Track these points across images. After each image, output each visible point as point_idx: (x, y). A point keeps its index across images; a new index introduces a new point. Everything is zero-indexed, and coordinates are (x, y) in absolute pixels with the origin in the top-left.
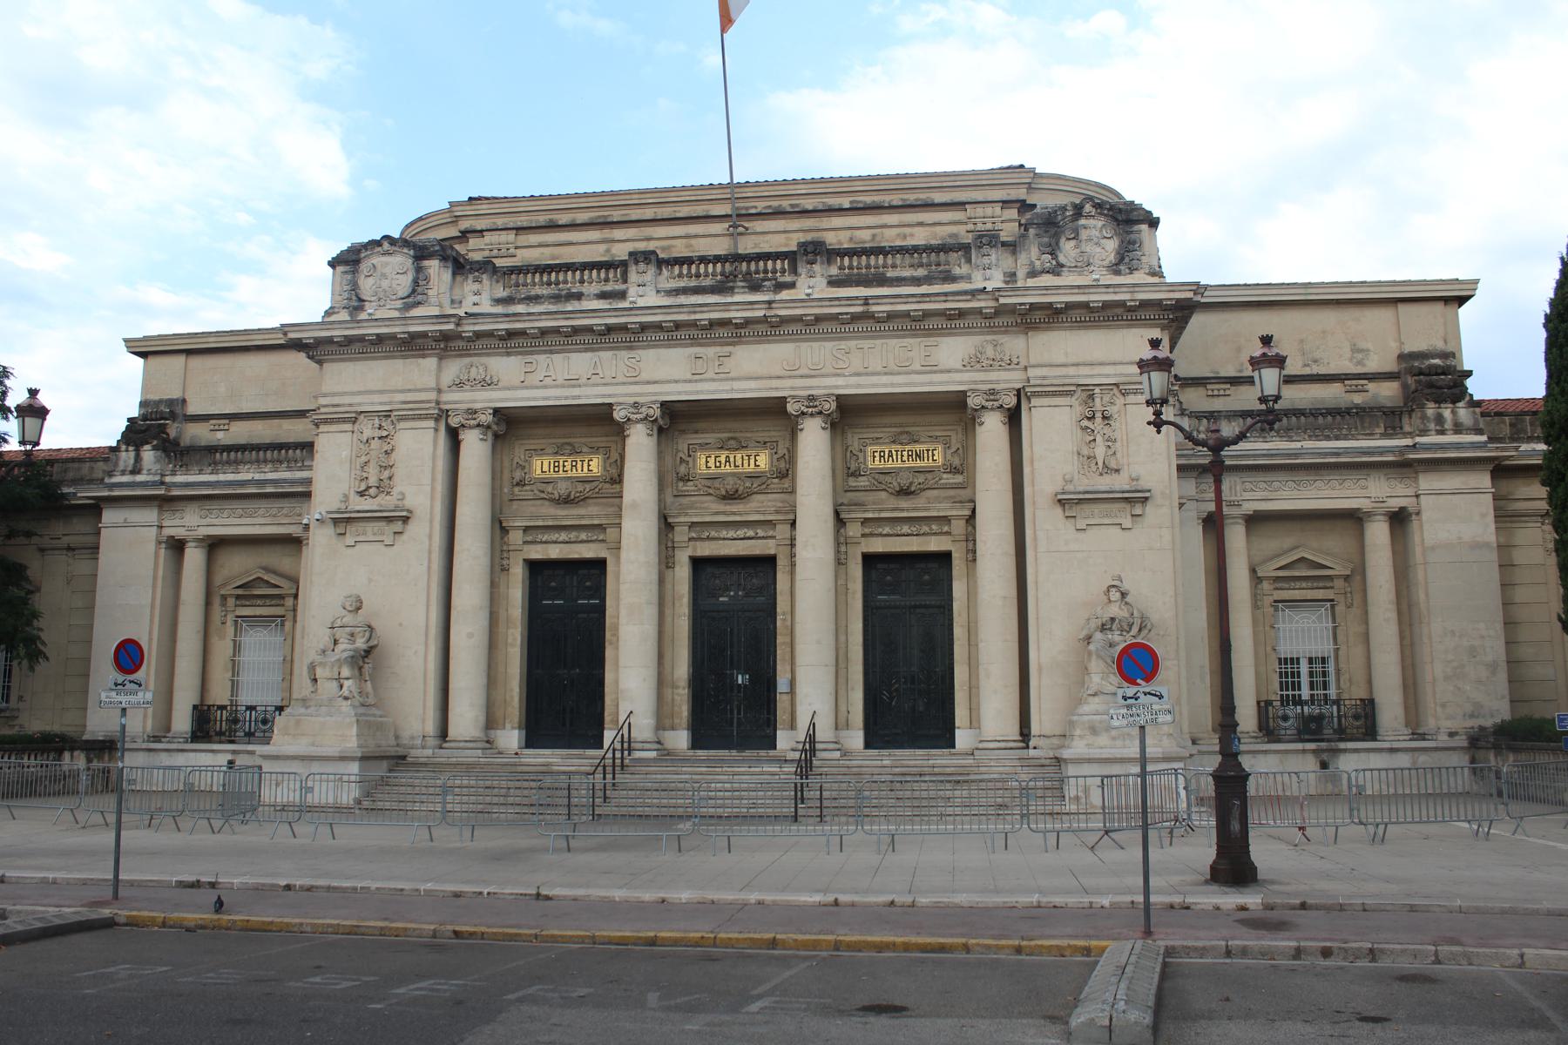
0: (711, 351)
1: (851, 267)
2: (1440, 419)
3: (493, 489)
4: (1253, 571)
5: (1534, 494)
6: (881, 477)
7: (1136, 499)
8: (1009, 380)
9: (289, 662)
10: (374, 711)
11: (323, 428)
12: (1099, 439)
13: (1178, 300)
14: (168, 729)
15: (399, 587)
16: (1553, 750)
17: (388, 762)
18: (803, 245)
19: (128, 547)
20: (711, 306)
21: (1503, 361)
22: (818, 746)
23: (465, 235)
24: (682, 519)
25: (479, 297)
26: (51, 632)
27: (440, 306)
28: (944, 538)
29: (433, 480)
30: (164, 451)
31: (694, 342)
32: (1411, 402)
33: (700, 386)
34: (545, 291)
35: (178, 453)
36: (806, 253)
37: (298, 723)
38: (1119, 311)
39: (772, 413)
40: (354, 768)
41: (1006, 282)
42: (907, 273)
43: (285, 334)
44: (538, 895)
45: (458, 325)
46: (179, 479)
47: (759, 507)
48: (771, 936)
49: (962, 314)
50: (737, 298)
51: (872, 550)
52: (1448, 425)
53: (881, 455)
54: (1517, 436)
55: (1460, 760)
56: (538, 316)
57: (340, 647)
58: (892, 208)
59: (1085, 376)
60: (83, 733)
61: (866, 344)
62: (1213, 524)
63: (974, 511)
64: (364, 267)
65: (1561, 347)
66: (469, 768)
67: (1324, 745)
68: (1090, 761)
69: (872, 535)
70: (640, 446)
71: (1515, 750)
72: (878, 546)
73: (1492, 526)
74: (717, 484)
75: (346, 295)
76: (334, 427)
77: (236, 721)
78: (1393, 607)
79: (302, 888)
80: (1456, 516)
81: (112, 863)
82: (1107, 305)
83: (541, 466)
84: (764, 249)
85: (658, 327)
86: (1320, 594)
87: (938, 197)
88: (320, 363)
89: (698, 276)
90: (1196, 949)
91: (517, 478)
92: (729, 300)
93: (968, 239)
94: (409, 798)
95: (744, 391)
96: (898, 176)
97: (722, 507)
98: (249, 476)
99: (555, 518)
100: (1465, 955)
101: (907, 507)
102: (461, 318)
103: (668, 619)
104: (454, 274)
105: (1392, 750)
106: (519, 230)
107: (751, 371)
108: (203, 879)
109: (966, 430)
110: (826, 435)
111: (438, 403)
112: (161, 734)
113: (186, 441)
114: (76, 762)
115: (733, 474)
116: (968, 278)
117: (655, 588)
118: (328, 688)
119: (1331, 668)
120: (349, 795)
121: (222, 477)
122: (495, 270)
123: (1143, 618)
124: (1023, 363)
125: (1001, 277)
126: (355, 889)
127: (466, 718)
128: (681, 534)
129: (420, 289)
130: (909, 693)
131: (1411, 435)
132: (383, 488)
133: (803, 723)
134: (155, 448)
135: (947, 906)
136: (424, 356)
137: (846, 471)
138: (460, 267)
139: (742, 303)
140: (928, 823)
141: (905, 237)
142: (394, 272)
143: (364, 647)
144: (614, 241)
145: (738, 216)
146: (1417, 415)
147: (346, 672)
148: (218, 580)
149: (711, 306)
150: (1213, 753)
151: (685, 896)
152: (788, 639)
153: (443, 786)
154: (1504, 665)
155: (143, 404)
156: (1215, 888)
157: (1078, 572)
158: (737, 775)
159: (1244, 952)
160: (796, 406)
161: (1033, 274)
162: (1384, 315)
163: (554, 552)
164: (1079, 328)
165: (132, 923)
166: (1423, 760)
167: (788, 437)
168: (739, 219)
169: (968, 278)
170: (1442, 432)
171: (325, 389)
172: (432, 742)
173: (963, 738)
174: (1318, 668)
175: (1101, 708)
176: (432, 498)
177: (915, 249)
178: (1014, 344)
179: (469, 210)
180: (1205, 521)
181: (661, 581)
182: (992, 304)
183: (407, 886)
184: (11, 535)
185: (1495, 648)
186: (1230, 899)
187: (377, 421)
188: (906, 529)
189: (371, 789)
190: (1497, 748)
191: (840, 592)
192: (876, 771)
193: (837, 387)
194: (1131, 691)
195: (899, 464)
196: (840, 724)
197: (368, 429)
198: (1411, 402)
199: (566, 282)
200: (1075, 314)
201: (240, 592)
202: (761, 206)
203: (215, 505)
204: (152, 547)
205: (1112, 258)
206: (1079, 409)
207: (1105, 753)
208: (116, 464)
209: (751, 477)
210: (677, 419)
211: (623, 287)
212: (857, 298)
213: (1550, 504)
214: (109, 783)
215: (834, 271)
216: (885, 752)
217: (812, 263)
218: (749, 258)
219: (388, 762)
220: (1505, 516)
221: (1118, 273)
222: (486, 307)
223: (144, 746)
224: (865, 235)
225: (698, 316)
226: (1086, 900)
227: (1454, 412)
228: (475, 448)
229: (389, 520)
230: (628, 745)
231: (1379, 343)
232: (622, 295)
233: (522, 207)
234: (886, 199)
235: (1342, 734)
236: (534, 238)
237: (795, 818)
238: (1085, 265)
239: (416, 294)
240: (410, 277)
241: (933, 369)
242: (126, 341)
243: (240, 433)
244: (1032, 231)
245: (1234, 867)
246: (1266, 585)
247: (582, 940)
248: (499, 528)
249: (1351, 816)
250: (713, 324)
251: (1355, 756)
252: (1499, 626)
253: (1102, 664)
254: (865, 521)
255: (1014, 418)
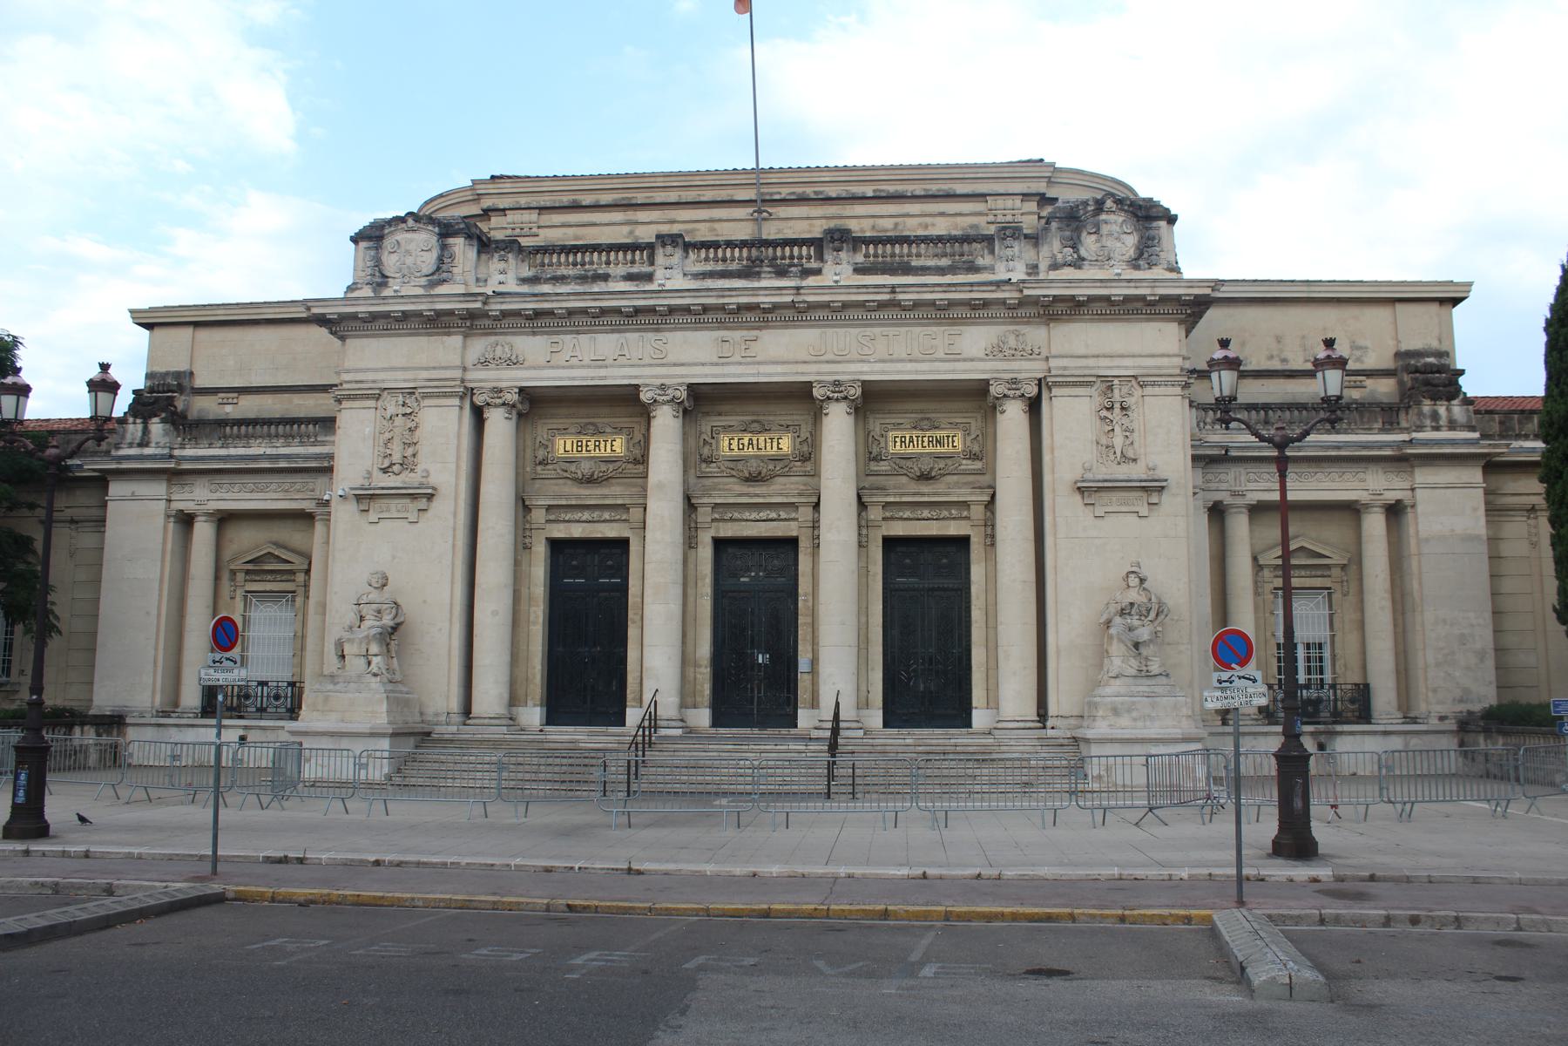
0: (737, 335)
1: (876, 256)
2: (1435, 416)
3: (517, 467)
4: (1255, 559)
5: (1531, 489)
6: (903, 463)
7: (1152, 488)
8: (1030, 369)
9: (300, 640)
10: (401, 687)
11: (345, 404)
12: (1117, 429)
13: (1196, 296)
14: (176, 704)
15: (418, 568)
16: (1544, 734)
17: (415, 738)
18: (830, 232)
19: (136, 521)
20: (739, 291)
21: (1501, 360)
22: (842, 725)
23: (487, 213)
24: (706, 500)
25: (504, 276)
26: (62, 603)
27: (466, 284)
28: (963, 522)
29: (458, 458)
30: (173, 423)
31: (721, 325)
32: (1407, 399)
33: (726, 370)
34: (571, 271)
35: (186, 426)
36: (833, 240)
37: (326, 699)
38: (1139, 305)
39: (799, 398)
40: (385, 744)
41: (1029, 274)
42: (931, 263)
43: (309, 309)
44: (630, 869)
45: (485, 303)
46: (189, 452)
47: (782, 489)
48: (882, 907)
49: (986, 304)
50: (764, 283)
51: (722, 534)
52: (1443, 422)
53: (902, 440)
54: (1506, 433)
55: (1450, 743)
56: (565, 296)
57: (366, 624)
58: (915, 198)
59: (1105, 367)
60: (89, 708)
61: (891, 331)
62: (1217, 513)
63: (993, 496)
64: (388, 243)
65: (1560, 351)
66: (495, 744)
67: (1321, 727)
68: (1112, 741)
69: (892, 518)
70: (666, 427)
71: (1505, 734)
72: (899, 529)
73: (1483, 520)
74: (740, 466)
75: (369, 271)
76: (357, 404)
77: (247, 697)
78: (1388, 596)
79: (391, 864)
80: (1449, 508)
81: (210, 841)
82: (1128, 299)
83: (563, 446)
84: (790, 233)
85: (686, 310)
86: (1318, 582)
87: (960, 188)
88: (343, 338)
89: (724, 260)
90: (1292, 917)
91: (540, 458)
92: (756, 284)
93: (992, 230)
94: (450, 774)
95: (770, 375)
96: (920, 167)
97: (745, 489)
98: (261, 451)
99: (578, 497)
100: (1545, 922)
101: (928, 492)
102: (488, 297)
103: (691, 599)
104: (479, 252)
105: (1386, 733)
106: (542, 209)
107: (777, 355)
108: (291, 855)
109: (985, 417)
110: (850, 420)
111: (463, 381)
112: (170, 709)
113: (193, 415)
114: (85, 737)
115: (756, 457)
116: (991, 269)
117: (680, 567)
118: (355, 664)
119: (1327, 654)
120: (378, 771)
121: (232, 451)
122: (520, 249)
123: (1160, 603)
124: (1044, 355)
125: (1024, 269)
126: (445, 864)
127: (490, 695)
128: (704, 515)
129: (445, 267)
130: (928, 671)
131: (1407, 430)
132: (407, 465)
133: (647, 697)
134: (163, 421)
135: (1032, 879)
136: (449, 334)
137: (869, 455)
138: (485, 245)
139: (769, 288)
140: (982, 800)
141: (926, 227)
142: (419, 248)
143: (391, 623)
144: (637, 223)
145: (764, 201)
146: (1413, 411)
147: (374, 648)
148: (227, 554)
149: (739, 291)
150: (1277, 734)
151: (775, 870)
152: (809, 620)
153: (500, 762)
154: (1492, 653)
155: (149, 376)
156: (1280, 861)
157: (1094, 556)
158: (755, 752)
159: (1337, 920)
160: (822, 391)
161: (1055, 266)
162: (1383, 313)
163: (577, 531)
164: (1099, 321)
165: (240, 897)
166: (1415, 742)
167: (811, 421)
168: (763, 205)
169: (991, 269)
170: (1437, 428)
171: (347, 365)
172: (457, 719)
173: (980, 718)
174: (1314, 653)
175: (1123, 690)
176: (457, 478)
177: (939, 239)
178: (1036, 335)
179: (492, 188)
180: (1210, 509)
181: (517, 563)
182: (1017, 295)
183: (497, 861)
184: (14, 506)
185: (1484, 637)
186: (1301, 872)
187: (401, 399)
188: (926, 513)
189: (401, 765)
190: (1487, 731)
191: (863, 573)
192: (900, 749)
193: (861, 373)
194: (1225, 676)
195: (920, 450)
196: (863, 704)
197: (391, 405)
198: (1407, 399)
199: (592, 263)
200: (1096, 307)
201: (250, 567)
202: (785, 192)
203: (226, 479)
204: (161, 520)
205: (1132, 253)
206: (1098, 400)
207: (1127, 734)
208: (123, 437)
209: (774, 459)
210: (702, 401)
211: (650, 269)
212: (884, 286)
213: (1547, 499)
214: (114, 758)
215: (860, 258)
216: (904, 731)
217: (839, 250)
218: (774, 244)
219: (415, 738)
220: (1495, 510)
221: (1137, 268)
222: (512, 286)
223: (154, 721)
224: (887, 224)
225: (726, 300)
226: (1166, 872)
227: (1448, 410)
228: (499, 426)
229: (413, 497)
230: (652, 722)
231: (1374, 341)
232: (649, 277)
233: (546, 186)
234: (908, 188)
235: (1337, 717)
236: (557, 218)
237: (828, 795)
238: (1105, 259)
239: (441, 272)
240: (435, 254)
241: (955, 357)
242: (132, 311)
243: (249, 406)
244: (1054, 225)
245: (1295, 841)
246: (1266, 573)
247: (696, 912)
248: (523, 506)
249: (1381, 795)
250: (741, 308)
251: (1351, 738)
252: (1488, 615)
253: (1123, 648)
254: (886, 505)
255: (1034, 406)
